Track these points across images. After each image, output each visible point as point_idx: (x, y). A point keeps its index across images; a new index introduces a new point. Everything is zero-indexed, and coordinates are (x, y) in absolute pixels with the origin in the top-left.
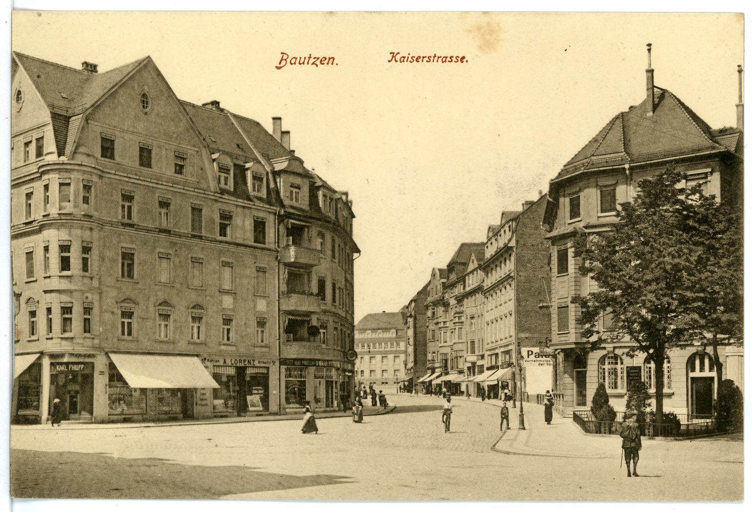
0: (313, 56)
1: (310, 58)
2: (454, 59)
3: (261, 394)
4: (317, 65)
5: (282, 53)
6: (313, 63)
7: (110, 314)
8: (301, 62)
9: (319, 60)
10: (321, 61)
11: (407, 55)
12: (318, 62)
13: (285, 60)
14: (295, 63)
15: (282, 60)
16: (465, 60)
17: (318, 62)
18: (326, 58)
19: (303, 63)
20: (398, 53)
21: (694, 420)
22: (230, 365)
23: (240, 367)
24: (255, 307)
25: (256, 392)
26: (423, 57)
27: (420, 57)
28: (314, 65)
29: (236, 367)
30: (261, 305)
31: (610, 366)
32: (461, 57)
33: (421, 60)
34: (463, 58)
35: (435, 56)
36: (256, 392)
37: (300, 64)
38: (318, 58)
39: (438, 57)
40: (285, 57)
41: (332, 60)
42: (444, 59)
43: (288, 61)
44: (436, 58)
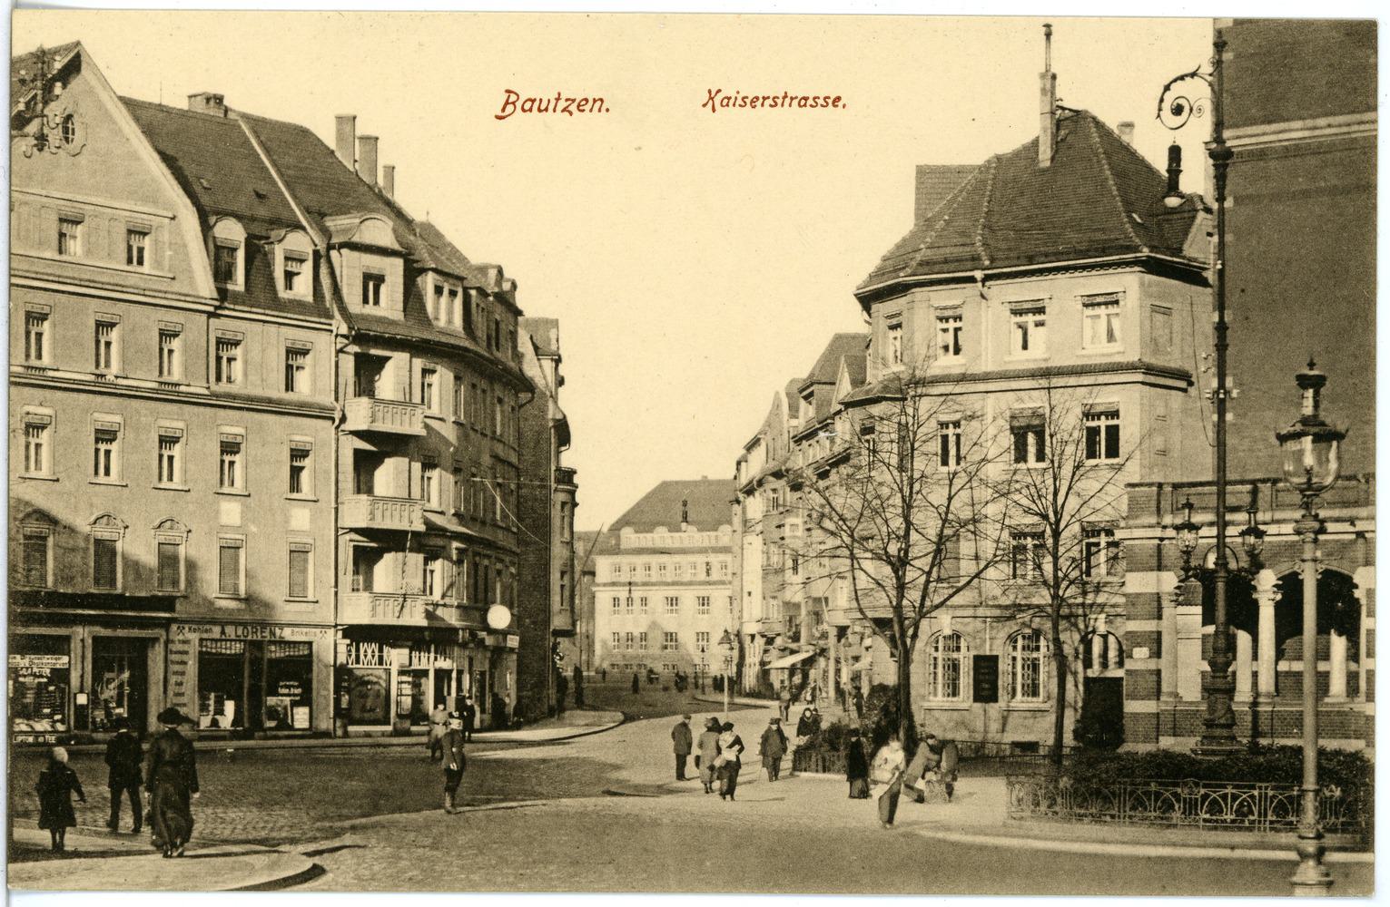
0: (563, 97)
1: (558, 99)
2: (821, 101)
3: (295, 695)
4: (571, 114)
5: (508, 91)
6: (563, 110)
7: (973, 552)
8: (543, 107)
9: (576, 104)
10: (579, 106)
11: (733, 95)
12: (573, 108)
13: (513, 103)
14: (530, 110)
15: (507, 103)
16: (840, 104)
17: (573, 108)
18: (587, 100)
19: (546, 110)
20: (719, 91)
21: (1130, 577)
22: (233, 637)
23: (252, 643)
24: (287, 522)
25: (286, 691)
26: (764, 98)
27: (757, 98)
28: (566, 114)
29: (245, 641)
30: (301, 518)
31: (1027, 654)
32: (833, 97)
33: (587, 108)
34: (838, 99)
35: (785, 97)
36: (286, 691)
37: (539, 110)
38: (574, 101)
39: (792, 99)
40: (513, 98)
41: (599, 103)
42: (803, 102)
43: (519, 104)
44: (788, 100)
